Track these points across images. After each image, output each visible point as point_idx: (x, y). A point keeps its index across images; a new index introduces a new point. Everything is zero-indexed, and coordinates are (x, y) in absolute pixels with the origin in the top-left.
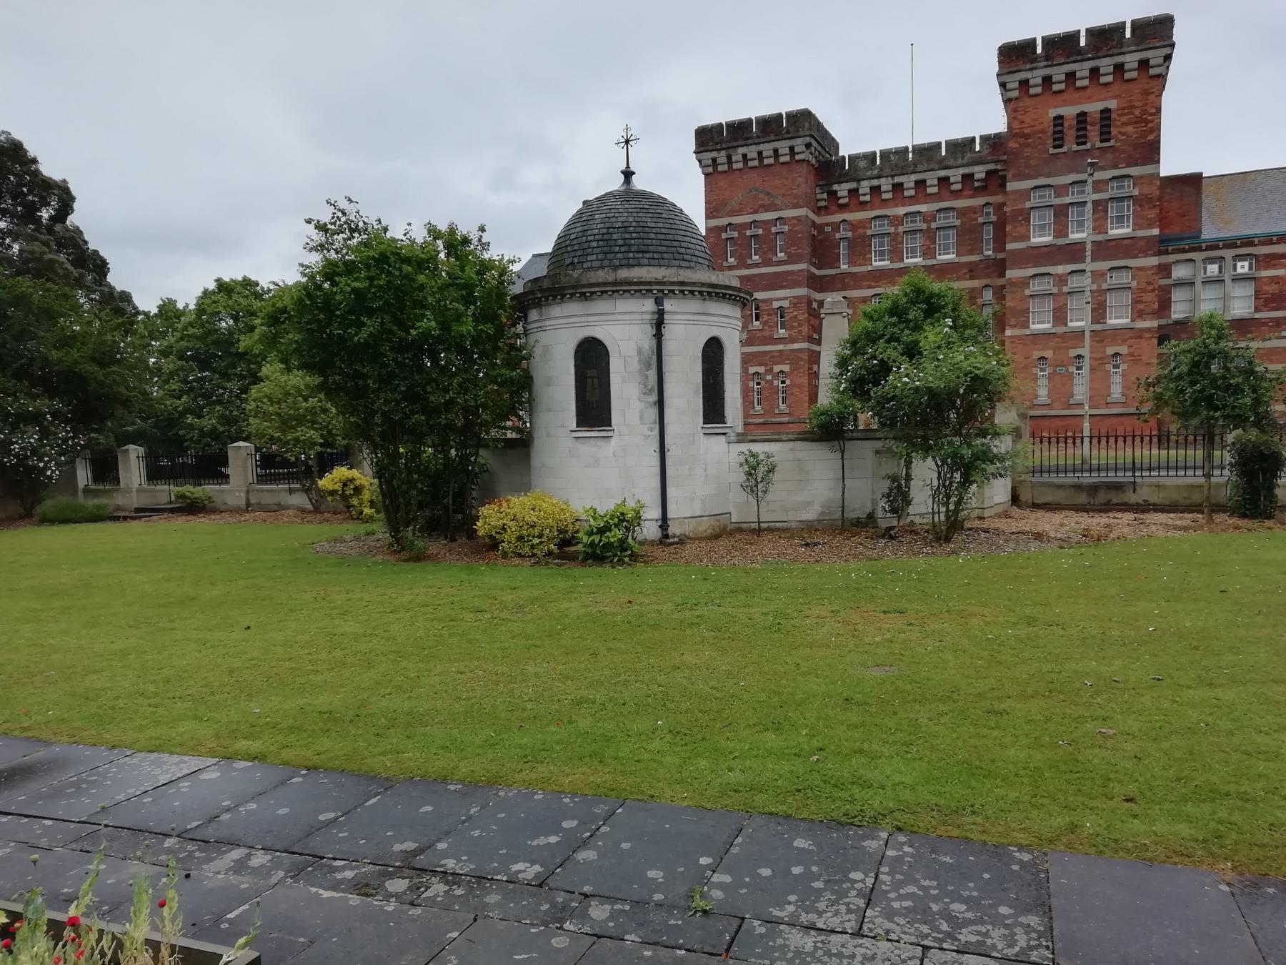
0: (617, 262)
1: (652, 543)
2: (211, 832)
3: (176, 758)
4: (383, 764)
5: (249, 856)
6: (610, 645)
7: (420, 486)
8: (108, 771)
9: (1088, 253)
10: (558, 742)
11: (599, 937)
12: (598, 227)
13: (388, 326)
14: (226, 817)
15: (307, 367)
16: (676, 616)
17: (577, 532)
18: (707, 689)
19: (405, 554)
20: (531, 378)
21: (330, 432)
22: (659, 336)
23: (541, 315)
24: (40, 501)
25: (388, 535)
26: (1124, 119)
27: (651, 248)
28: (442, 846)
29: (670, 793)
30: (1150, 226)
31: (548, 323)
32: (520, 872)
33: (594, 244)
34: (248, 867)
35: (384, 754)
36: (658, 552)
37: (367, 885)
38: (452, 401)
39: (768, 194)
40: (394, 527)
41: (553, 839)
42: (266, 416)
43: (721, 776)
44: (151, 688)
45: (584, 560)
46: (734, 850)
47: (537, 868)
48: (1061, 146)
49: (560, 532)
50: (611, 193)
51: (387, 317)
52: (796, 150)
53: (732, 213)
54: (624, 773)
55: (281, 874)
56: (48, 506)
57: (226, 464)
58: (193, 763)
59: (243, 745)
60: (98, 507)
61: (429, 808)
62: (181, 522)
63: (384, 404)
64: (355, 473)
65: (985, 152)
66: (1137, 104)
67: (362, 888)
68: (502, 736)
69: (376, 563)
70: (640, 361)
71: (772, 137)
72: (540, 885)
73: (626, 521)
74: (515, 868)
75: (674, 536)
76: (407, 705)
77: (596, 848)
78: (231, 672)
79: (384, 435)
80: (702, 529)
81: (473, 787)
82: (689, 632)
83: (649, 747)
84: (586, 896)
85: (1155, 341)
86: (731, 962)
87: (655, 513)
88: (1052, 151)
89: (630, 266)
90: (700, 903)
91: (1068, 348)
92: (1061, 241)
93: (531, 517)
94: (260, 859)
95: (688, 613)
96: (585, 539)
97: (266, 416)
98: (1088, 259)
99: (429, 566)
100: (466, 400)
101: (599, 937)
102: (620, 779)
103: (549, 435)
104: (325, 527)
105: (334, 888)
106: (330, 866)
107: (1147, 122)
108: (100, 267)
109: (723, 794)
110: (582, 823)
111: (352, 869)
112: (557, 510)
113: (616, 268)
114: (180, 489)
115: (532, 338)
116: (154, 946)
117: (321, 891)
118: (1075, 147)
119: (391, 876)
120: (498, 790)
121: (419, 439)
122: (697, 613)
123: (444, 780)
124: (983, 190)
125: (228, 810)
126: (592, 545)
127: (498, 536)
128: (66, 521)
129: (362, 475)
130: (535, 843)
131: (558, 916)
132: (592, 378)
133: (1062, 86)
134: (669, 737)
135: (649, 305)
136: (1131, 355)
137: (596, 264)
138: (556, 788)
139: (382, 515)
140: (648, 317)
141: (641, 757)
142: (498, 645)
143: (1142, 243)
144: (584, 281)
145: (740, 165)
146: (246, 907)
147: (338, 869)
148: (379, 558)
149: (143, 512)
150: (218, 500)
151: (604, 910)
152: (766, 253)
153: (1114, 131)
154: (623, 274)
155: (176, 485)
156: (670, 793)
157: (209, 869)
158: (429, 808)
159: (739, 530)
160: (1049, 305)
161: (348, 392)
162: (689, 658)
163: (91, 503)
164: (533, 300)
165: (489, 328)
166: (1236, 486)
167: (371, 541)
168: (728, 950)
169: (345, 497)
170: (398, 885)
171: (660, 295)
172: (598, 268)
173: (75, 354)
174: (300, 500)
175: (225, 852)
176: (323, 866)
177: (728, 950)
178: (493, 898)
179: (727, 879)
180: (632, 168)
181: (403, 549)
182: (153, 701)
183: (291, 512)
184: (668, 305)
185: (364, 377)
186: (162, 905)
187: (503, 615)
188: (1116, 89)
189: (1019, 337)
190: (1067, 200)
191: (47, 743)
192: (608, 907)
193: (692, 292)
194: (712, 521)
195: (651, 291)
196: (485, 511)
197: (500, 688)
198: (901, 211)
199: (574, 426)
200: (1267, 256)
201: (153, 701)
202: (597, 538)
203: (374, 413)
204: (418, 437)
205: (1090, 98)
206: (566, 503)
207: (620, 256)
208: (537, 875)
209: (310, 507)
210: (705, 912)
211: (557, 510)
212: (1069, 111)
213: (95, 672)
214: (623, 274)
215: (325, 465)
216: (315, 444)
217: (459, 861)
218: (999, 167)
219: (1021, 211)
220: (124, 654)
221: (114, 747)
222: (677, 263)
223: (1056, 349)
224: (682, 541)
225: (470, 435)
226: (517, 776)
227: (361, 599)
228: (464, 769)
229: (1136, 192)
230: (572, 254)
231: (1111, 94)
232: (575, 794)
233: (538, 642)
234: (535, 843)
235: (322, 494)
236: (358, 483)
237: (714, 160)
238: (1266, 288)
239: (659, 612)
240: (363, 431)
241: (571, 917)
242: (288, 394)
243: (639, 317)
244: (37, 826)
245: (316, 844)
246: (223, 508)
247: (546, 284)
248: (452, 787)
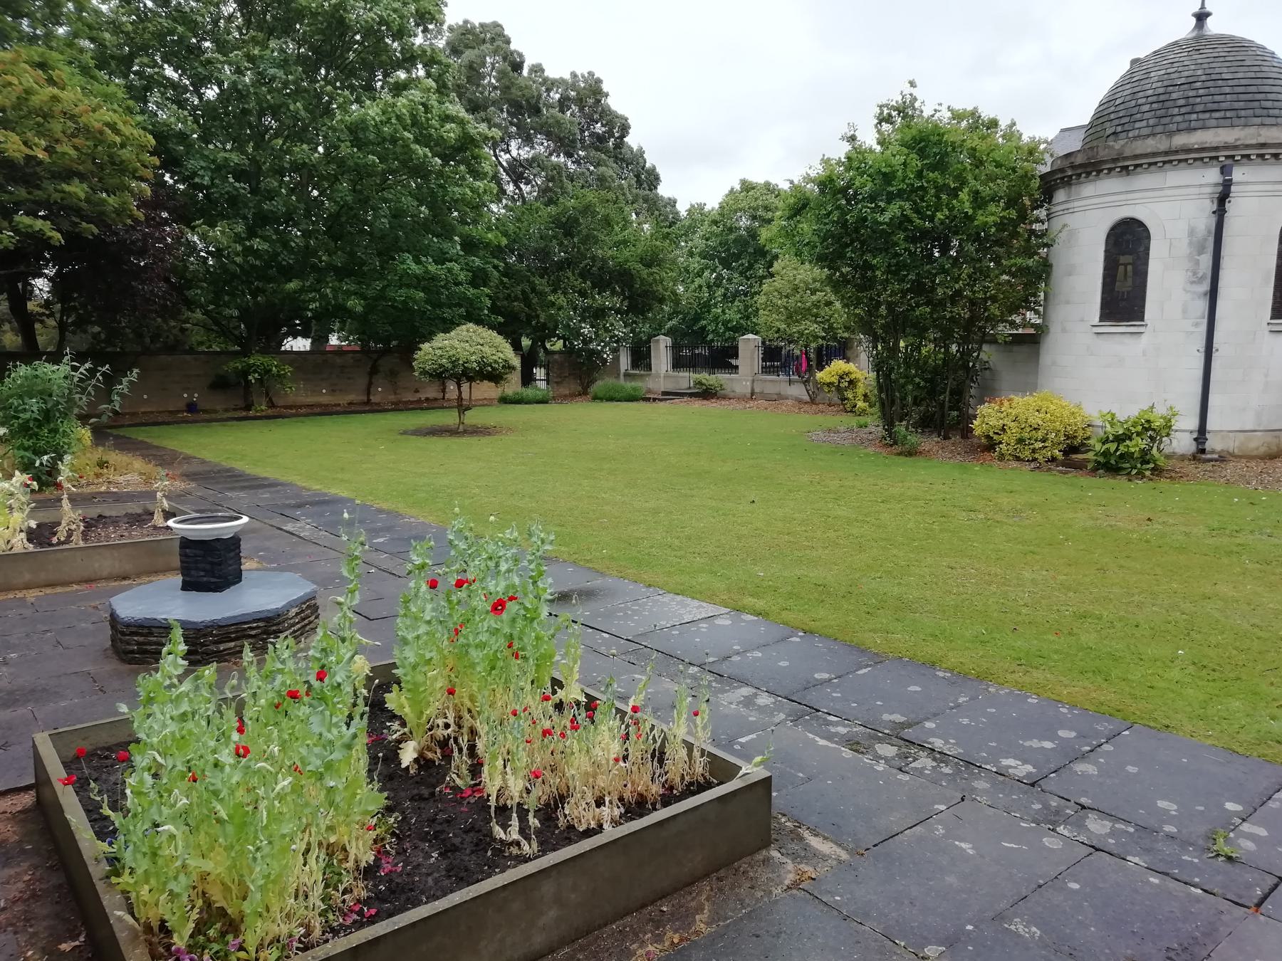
0: (1174, 127)
1: (1183, 458)
2: (724, 668)
3: (696, 603)
4: (875, 641)
5: (755, 695)
6: (1122, 562)
7: (917, 380)
8: (646, 604)
10: (1056, 652)
11: (1097, 850)
12: (1154, 85)
13: (908, 212)
14: (736, 658)
15: (821, 260)
16: (1210, 541)
17: (1088, 438)
18: (1246, 626)
19: (898, 448)
20: (1051, 266)
21: (831, 327)
22: (1220, 213)
23: (1069, 195)
24: (593, 381)
25: (880, 429)
27: (1224, 106)
28: (929, 725)
29: (1190, 727)
31: (1076, 204)
32: (1011, 767)
33: (1146, 108)
34: (755, 704)
35: (874, 631)
36: (1190, 468)
37: (858, 743)
38: (958, 293)
40: (889, 422)
41: (1048, 745)
42: (775, 308)
43: (1259, 722)
44: (677, 542)
45: (1095, 470)
46: (1271, 804)
47: (1029, 768)
49: (1067, 437)
50: (1175, 44)
51: (907, 205)
54: (1134, 697)
55: (782, 716)
56: (599, 386)
57: (736, 355)
58: (709, 610)
59: (749, 601)
60: (635, 389)
61: (918, 689)
62: (697, 405)
63: (890, 296)
64: (851, 367)
67: (854, 744)
68: (995, 635)
69: (867, 455)
70: (1190, 243)
72: (1033, 785)
73: (1152, 430)
74: (1005, 762)
75: (1213, 452)
76: (896, 590)
77: (1096, 763)
78: (739, 538)
79: (888, 328)
80: (1253, 445)
81: (961, 677)
82: (1225, 561)
83: (1166, 676)
84: (1083, 807)
86: (1262, 918)
87: (1193, 423)
89: (1191, 130)
90: (1221, 845)
93: (1035, 419)
94: (764, 700)
95: (1226, 540)
96: (1098, 447)
97: (775, 308)
99: (920, 462)
100: (974, 292)
101: (1097, 850)
102: (1128, 701)
103: (1064, 330)
104: (820, 418)
105: (829, 737)
106: (825, 720)
108: (652, 179)
109: (1260, 742)
110: (1082, 736)
111: (845, 726)
112: (1066, 413)
113: (1171, 134)
114: (697, 376)
115: (1057, 223)
116: (690, 747)
117: (817, 739)
119: (880, 740)
120: (988, 686)
121: (921, 331)
122: (1238, 541)
123: (933, 664)
125: (738, 653)
126: (1106, 454)
127: (995, 437)
128: (611, 399)
129: (859, 368)
130: (1027, 744)
131: (1051, 820)
132: (1126, 265)
134: (1191, 669)
135: (1212, 175)
137: (1146, 131)
138: (1053, 696)
139: (876, 409)
140: (1209, 190)
141: (1155, 684)
142: (991, 546)
144: (1127, 153)
146: (754, 736)
147: (831, 723)
148: (871, 450)
149: (668, 395)
150: (728, 388)
151: (1104, 826)
154: (1180, 140)
155: (695, 372)
156: (1190, 727)
157: (725, 699)
158: (918, 689)
161: (856, 287)
162: (1223, 589)
163: (630, 385)
164: (1062, 178)
165: (1013, 214)
167: (863, 433)
168: (1259, 905)
169: (839, 389)
170: (888, 750)
171: (1229, 162)
172: (1148, 136)
173: (626, 253)
174: (798, 391)
175: (736, 688)
176: (818, 718)
177: (1259, 905)
178: (981, 784)
179: (1262, 832)
180: (1208, 8)
181: (895, 443)
182: (679, 554)
183: (790, 402)
184: (1238, 174)
185: (873, 268)
186: (696, 714)
187: (998, 517)
191: (603, 574)
192: (1108, 824)
193: (1262, 156)
194: (1269, 438)
195: (1217, 158)
196: (984, 409)
197: (993, 588)
199: (1096, 320)
201: (679, 554)
202: (1113, 447)
203: (879, 304)
204: (920, 331)
206: (1079, 406)
207: (1179, 119)
208: (1029, 775)
209: (807, 398)
210: (1229, 858)
211: (1066, 413)
213: (634, 524)
214: (1180, 140)
215: (823, 357)
216: (817, 337)
217: (947, 742)
220: (656, 512)
221: (650, 586)
222: (1258, 120)
224: (1223, 458)
225: (974, 329)
226: (1009, 676)
227: (854, 487)
228: (953, 659)
230: (1117, 122)
232: (1074, 706)
233: (1036, 550)
234: (1027, 744)
235: (820, 386)
236: (853, 376)
239: (1186, 534)
240: (866, 326)
241: (1065, 822)
242: (796, 289)
243: (1196, 190)
244: (598, 635)
245: (812, 697)
246: (732, 395)
247: (1079, 160)
248: (941, 674)
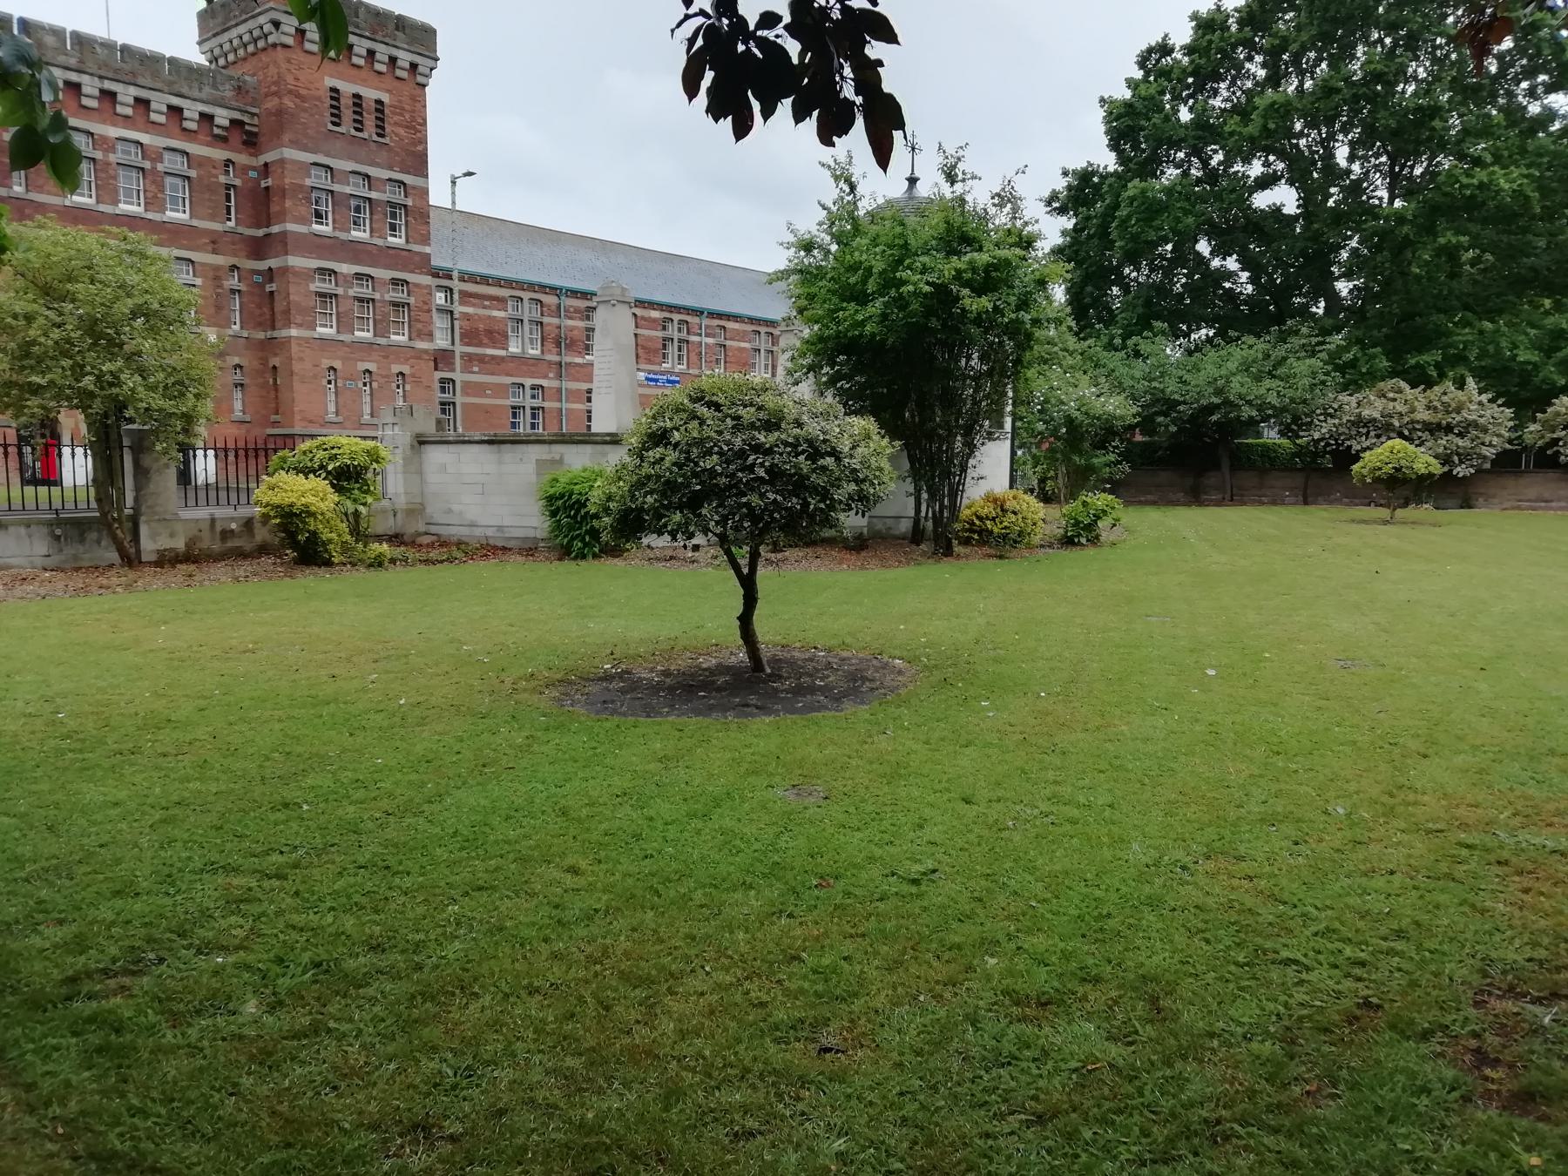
26: (396, 118)
48: (338, 125)
88: (331, 127)
118: (353, 132)
124: (222, 140)
136: (413, 376)
153: (388, 129)
159: (495, 548)
166: (1488, 497)
180: (917, 174)
188: (389, 82)
189: (307, 340)
198: (113, 132)
205: (365, 80)
218: (246, 119)
219: (301, 186)
223: (344, 359)
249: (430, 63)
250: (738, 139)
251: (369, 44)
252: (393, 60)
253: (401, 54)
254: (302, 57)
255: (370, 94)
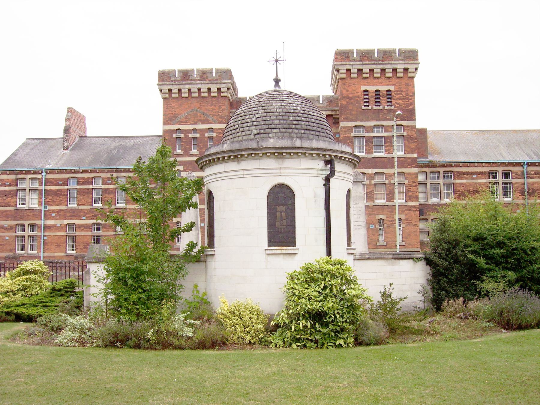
9: (396, 164)
26: (398, 96)
27: (315, 128)
30: (413, 152)
39: (204, 113)
52: (222, 90)
53: (180, 123)
65: (325, 105)
66: (404, 90)
71: (207, 82)
85: (418, 213)
88: (363, 108)
91: (375, 214)
92: (370, 156)
98: (396, 167)
107: (409, 99)
118: (375, 108)
132: (281, 212)
133: (367, 75)
136: (406, 219)
143: (409, 160)
145: (187, 95)
152: (201, 148)
160: (384, 190)
188: (394, 80)
190: (372, 134)
199: (266, 247)
200: (458, 172)
205: (381, 83)
212: (372, 89)
218: (333, 113)
219: (349, 137)
229: (405, 134)
231: (391, 83)
237: (170, 90)
238: (459, 189)
243: (316, 172)
249: (415, 66)
250: (70, 110)
251: (177, 87)
252: (395, 70)
253: (398, 66)
254: (352, 81)
255: (383, 88)
